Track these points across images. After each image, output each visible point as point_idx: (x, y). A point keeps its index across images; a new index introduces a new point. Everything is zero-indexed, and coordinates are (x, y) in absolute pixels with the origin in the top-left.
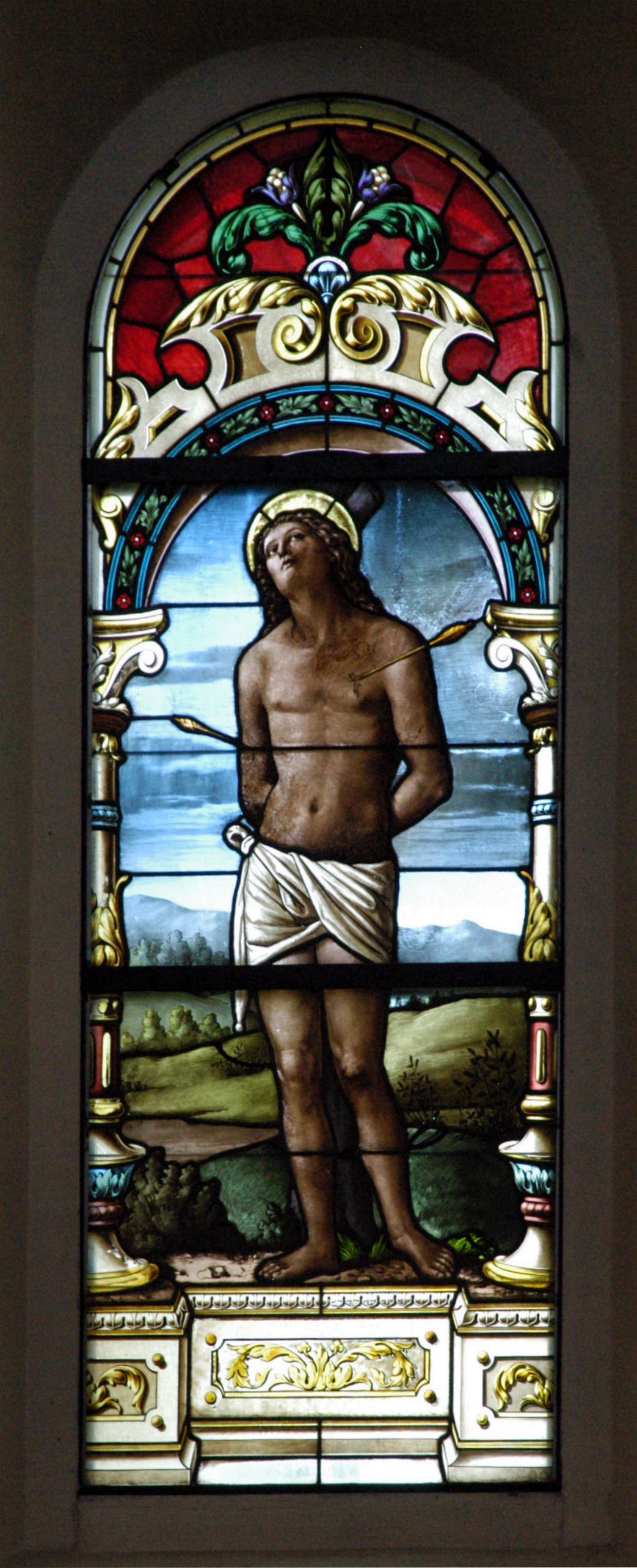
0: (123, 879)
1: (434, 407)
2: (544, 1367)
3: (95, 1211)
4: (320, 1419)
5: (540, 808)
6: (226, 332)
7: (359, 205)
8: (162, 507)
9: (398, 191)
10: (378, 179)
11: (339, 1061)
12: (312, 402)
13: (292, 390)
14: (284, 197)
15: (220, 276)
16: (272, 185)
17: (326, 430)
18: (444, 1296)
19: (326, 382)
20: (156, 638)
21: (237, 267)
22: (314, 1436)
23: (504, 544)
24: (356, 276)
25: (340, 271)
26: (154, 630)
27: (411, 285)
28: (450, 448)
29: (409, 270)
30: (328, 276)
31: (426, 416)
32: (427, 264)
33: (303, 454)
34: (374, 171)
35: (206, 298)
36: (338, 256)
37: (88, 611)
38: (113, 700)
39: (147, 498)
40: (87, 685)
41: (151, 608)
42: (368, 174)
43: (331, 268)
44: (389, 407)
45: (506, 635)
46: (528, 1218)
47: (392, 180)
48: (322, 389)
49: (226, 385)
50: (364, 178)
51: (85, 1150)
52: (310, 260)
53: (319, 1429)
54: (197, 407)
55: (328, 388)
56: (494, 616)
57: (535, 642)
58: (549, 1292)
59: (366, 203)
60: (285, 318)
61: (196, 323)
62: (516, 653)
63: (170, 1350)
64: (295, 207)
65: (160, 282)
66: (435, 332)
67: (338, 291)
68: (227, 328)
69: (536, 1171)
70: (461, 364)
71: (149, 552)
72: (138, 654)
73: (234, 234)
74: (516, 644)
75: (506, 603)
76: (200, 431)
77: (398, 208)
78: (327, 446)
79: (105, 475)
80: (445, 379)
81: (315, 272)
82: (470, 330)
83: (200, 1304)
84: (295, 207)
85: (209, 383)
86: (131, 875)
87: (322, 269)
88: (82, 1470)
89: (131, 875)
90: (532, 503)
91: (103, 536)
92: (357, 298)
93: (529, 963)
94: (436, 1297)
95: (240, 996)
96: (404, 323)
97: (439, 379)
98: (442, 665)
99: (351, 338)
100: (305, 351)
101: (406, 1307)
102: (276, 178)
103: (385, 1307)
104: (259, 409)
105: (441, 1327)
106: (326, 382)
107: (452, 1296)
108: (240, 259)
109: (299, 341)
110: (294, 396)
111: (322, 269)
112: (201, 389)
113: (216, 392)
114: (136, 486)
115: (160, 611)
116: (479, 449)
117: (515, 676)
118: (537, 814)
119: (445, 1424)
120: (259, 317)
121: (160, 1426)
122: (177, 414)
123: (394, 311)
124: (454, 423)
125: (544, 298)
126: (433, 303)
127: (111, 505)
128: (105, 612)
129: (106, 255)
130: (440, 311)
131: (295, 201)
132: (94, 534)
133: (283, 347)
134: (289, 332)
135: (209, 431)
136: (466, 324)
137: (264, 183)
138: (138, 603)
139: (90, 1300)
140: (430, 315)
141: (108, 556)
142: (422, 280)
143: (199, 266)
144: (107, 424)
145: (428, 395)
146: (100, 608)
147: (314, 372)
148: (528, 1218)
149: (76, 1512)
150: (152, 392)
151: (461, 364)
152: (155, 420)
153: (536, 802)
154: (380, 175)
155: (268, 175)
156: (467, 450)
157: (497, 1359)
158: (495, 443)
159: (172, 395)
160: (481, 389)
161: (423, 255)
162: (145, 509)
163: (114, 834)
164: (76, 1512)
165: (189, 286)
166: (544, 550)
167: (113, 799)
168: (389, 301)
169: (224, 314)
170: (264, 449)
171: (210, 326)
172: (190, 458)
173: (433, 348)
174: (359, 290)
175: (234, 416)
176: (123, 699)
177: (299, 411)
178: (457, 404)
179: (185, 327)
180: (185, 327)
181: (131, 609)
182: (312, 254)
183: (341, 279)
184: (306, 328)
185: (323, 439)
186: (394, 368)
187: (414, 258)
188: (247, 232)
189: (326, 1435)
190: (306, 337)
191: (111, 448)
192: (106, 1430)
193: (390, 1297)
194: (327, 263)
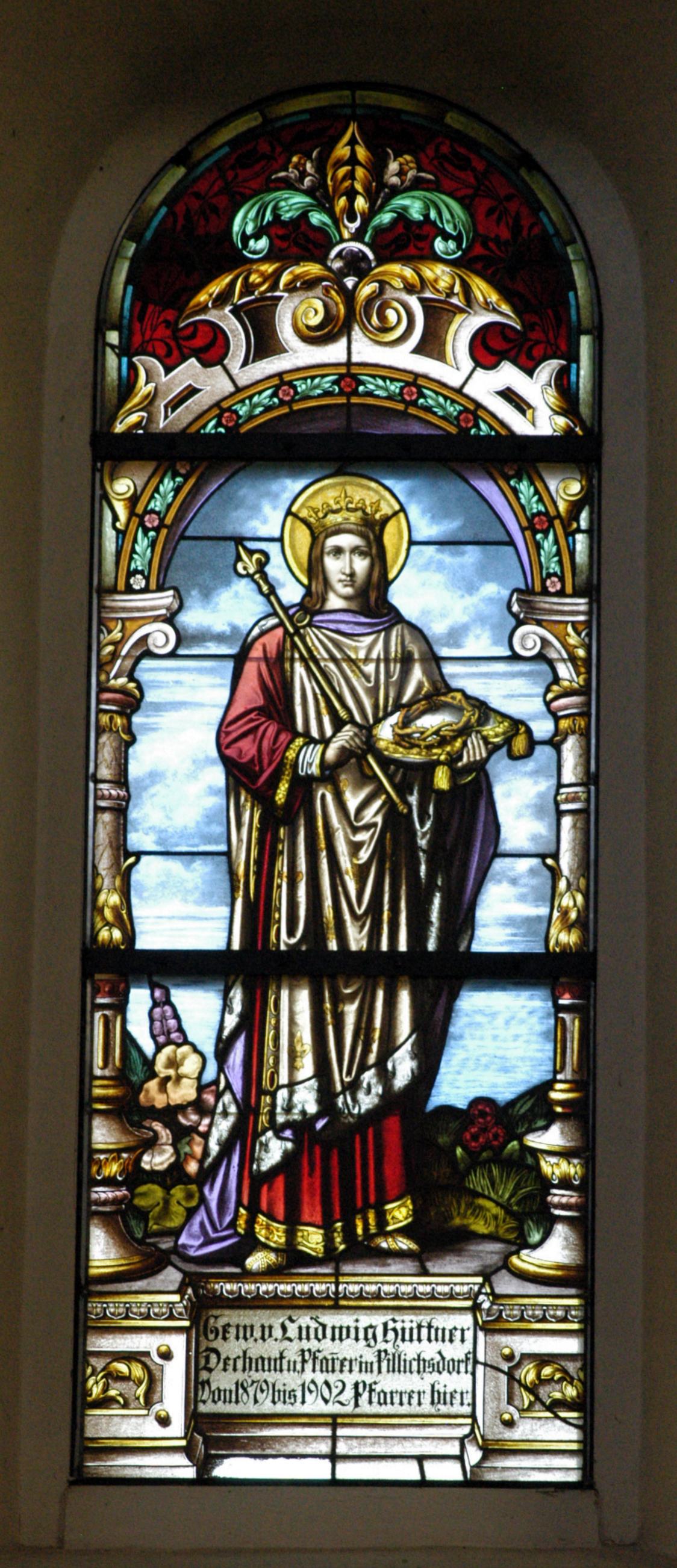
0: (132, 860)
1: (459, 391)
2: (572, 1367)
3: (94, 1196)
8: (177, 490)
11: (401, 1249)
19: (349, 364)
20: (170, 619)
23: (528, 533)
31: (453, 401)
36: (362, 242)
38: (122, 681)
39: (161, 481)
46: (557, 1212)
48: (343, 370)
49: (245, 363)
51: (83, 1133)
54: (214, 384)
55: (349, 370)
58: (577, 1278)
61: (214, 305)
62: (545, 642)
63: (178, 1344)
79: (113, 451)
86: (139, 855)
89: (139, 855)
95: (113, 381)
97: (467, 364)
98: (519, 996)
105: (467, 1320)
106: (349, 364)
110: (313, 378)
112: (219, 367)
116: (503, 432)
119: (469, 1421)
120: (280, 298)
121: (164, 1421)
122: (192, 391)
124: (479, 405)
139: (85, 1285)
145: (455, 381)
148: (557, 1212)
149: (63, 1500)
150: (168, 370)
151: (488, 349)
153: (563, 790)
156: (493, 433)
157: (524, 1356)
158: (520, 425)
159: (190, 371)
160: (508, 375)
162: (159, 493)
163: (121, 811)
164: (63, 1500)
166: (570, 539)
167: (122, 779)
176: (131, 678)
178: (485, 386)
192: (105, 1424)
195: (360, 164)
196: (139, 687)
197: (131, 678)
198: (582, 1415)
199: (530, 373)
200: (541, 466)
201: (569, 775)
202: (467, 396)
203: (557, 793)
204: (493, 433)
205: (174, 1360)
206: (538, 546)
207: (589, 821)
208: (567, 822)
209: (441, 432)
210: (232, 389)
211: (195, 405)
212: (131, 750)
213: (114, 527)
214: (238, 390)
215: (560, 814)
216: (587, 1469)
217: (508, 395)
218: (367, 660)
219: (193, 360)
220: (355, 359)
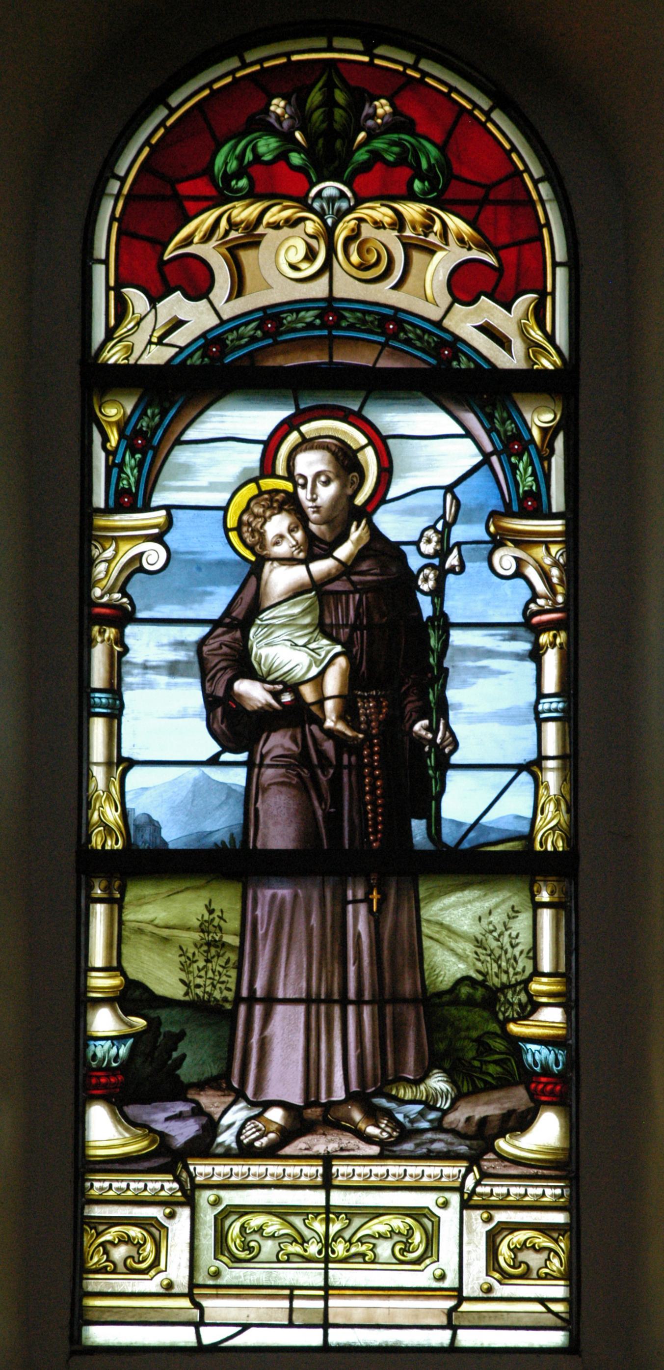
4: (292, 1288)
5: (546, 706)
6: (228, 249)
7: (362, 135)
9: (399, 123)
10: (380, 111)
12: (256, 329)
13: (297, 306)
14: (286, 125)
15: (223, 196)
16: (274, 112)
17: (330, 343)
18: (455, 1171)
20: (159, 539)
21: (240, 190)
22: (320, 1304)
24: (360, 201)
25: (342, 195)
26: (156, 531)
27: (412, 211)
28: (455, 363)
29: (412, 197)
30: (331, 200)
31: (431, 333)
32: (430, 193)
33: (299, 365)
34: (377, 103)
35: (209, 218)
37: (87, 511)
40: (86, 581)
41: (147, 507)
42: (370, 106)
43: (334, 192)
44: (390, 323)
45: (509, 544)
47: (396, 111)
50: (368, 110)
52: (313, 185)
53: (291, 1298)
54: (197, 318)
56: (496, 526)
57: (540, 552)
58: (558, 1166)
59: (368, 133)
60: (287, 239)
61: (198, 235)
64: (298, 135)
65: (161, 202)
66: (439, 255)
67: (340, 216)
68: (228, 246)
69: (544, 1051)
70: (464, 285)
71: (150, 454)
72: (142, 554)
73: (237, 158)
74: (519, 553)
75: (509, 513)
76: (201, 342)
77: (400, 139)
78: (331, 357)
80: (449, 299)
81: (319, 194)
82: (475, 254)
83: (201, 1174)
84: (298, 135)
85: (211, 296)
87: (325, 194)
88: (76, 1337)
90: (532, 420)
91: (106, 439)
92: (361, 220)
93: (540, 852)
94: (447, 1171)
96: (408, 246)
97: (445, 299)
99: (355, 258)
100: (309, 270)
101: (348, 1180)
102: (278, 106)
103: (308, 1179)
104: (262, 322)
107: (463, 1170)
108: (243, 183)
109: (302, 261)
110: (298, 311)
111: (325, 194)
112: (205, 301)
113: (220, 304)
114: (141, 390)
115: (163, 513)
117: (520, 582)
118: (543, 712)
122: (177, 324)
123: (396, 233)
125: (548, 224)
126: (437, 227)
127: (112, 412)
128: (108, 511)
129: (107, 172)
130: (445, 233)
131: (298, 129)
132: (97, 438)
133: (285, 265)
134: (293, 250)
135: (210, 341)
136: (470, 249)
137: (267, 111)
138: (140, 504)
140: (432, 238)
141: (111, 458)
142: (426, 207)
143: (201, 187)
144: (110, 333)
145: (434, 314)
146: (102, 505)
147: (318, 289)
152: (154, 330)
153: (542, 701)
154: (382, 106)
155: (270, 105)
156: (472, 366)
159: (175, 304)
160: (488, 310)
161: (426, 183)
165: (190, 206)
168: (392, 226)
169: (227, 233)
170: (271, 360)
171: (213, 243)
172: (192, 366)
173: (437, 269)
174: (361, 213)
175: (237, 328)
177: (303, 325)
178: (464, 323)
179: (188, 241)
180: (188, 241)
181: (133, 509)
182: (314, 180)
183: (344, 205)
184: (309, 248)
185: (327, 351)
186: (396, 287)
187: (417, 185)
188: (249, 156)
189: (297, 1303)
190: (311, 255)
191: (114, 356)
193: (401, 1170)
194: (330, 188)
195: (339, 106)
196: (132, 603)
197: (125, 594)
198: (568, 1283)
199: (508, 308)
200: (517, 397)
201: (551, 684)
202: (446, 331)
203: (537, 703)
204: (472, 366)
205: (177, 1219)
206: (514, 467)
207: (569, 720)
208: (546, 916)
209: (423, 366)
210: (216, 321)
211: (180, 338)
212: (177, 448)
213: (104, 448)
214: (223, 322)
215: (540, 722)
216: (573, 1063)
217: (486, 329)
218: (399, 223)
219: (179, 292)
220: (337, 294)
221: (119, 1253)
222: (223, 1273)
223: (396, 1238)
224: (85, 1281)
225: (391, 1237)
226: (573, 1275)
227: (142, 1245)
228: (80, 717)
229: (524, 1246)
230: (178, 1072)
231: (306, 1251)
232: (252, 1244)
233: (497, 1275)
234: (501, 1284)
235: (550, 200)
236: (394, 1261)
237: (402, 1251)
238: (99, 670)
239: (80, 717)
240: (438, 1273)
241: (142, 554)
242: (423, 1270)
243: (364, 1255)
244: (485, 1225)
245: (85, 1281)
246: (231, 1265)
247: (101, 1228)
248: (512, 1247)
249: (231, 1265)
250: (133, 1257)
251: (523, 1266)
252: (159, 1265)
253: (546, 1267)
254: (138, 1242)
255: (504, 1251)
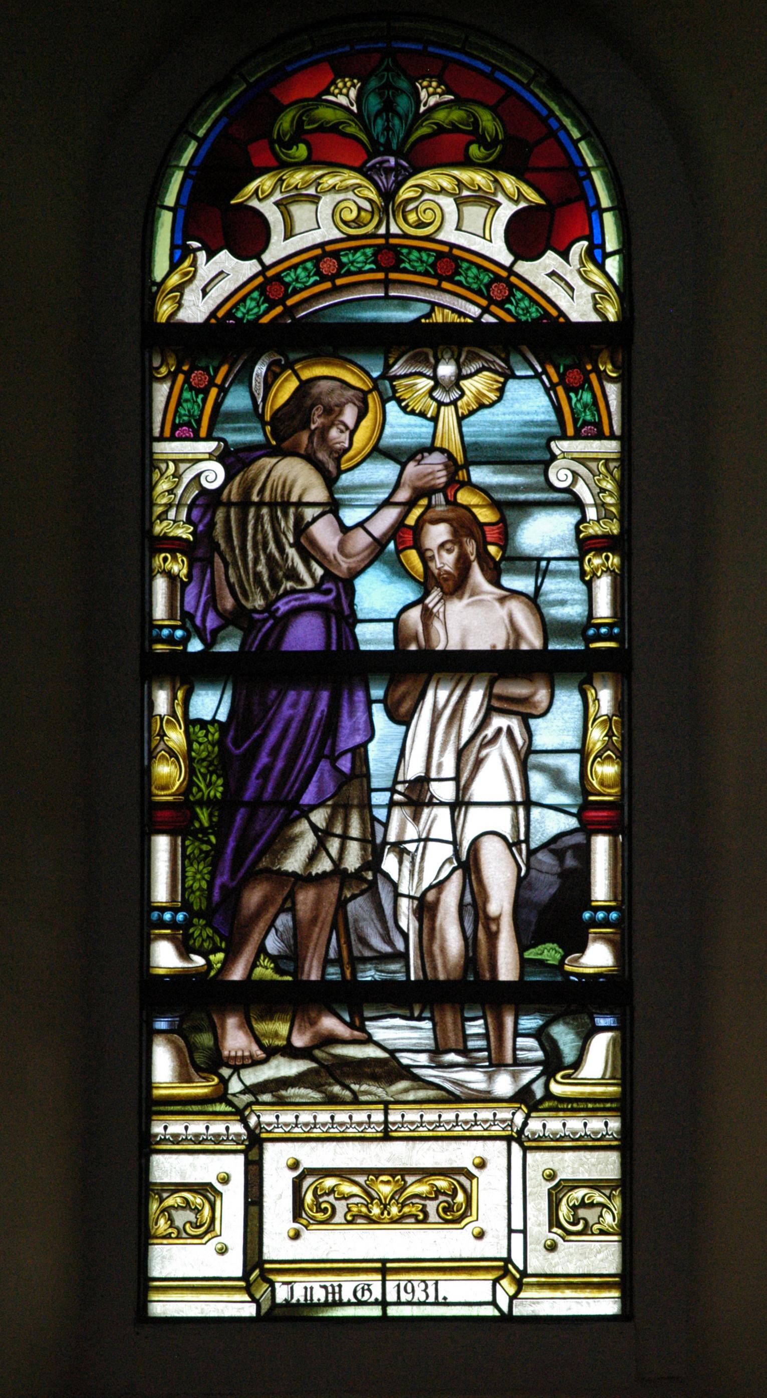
128: (162, 439)
221: (182, 1218)
222: (302, 1233)
223: (442, 1198)
224: (150, 1247)
225: (436, 1198)
226: (627, 1231)
227: (199, 1211)
228: (143, 382)
229: (583, 1204)
230: (343, 866)
231: (370, 1212)
232: (323, 1206)
233: (560, 1231)
234: (565, 1241)
235: (360, 702)
236: (441, 1221)
237: (445, 1210)
238: (176, 180)
239: (143, 382)
240: (476, 1231)
241: (198, 476)
242: (462, 1228)
243: (416, 1216)
244: (548, 1183)
245: (315, 1301)
246: (474, 1217)
247: (165, 1195)
248: (571, 1205)
249: (474, 1217)
250: (190, 1222)
251: (582, 1222)
252: (214, 1230)
253: (599, 1223)
254: (196, 1208)
255: (564, 1211)
